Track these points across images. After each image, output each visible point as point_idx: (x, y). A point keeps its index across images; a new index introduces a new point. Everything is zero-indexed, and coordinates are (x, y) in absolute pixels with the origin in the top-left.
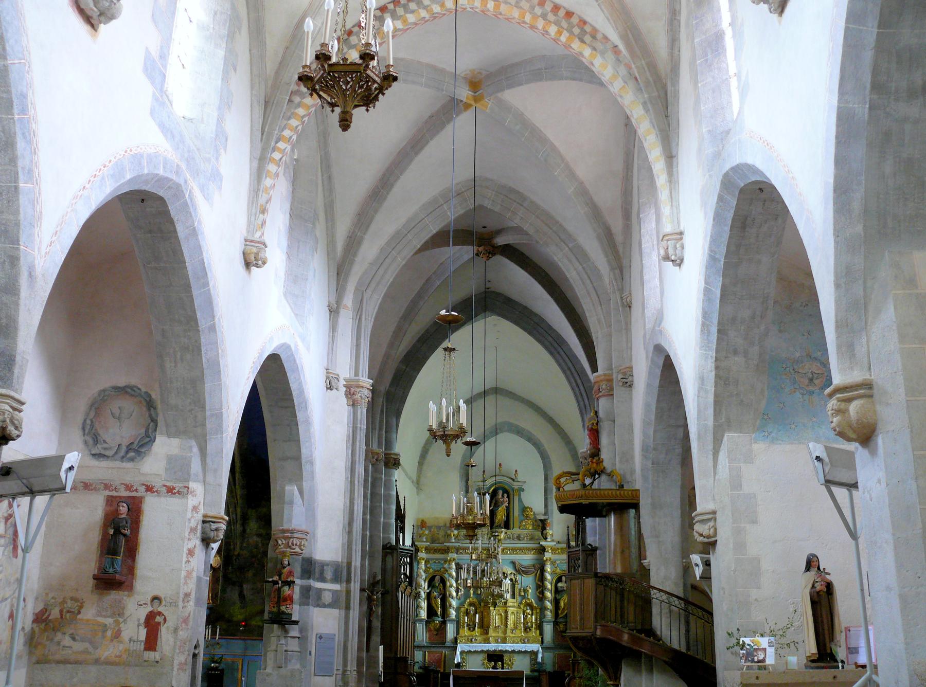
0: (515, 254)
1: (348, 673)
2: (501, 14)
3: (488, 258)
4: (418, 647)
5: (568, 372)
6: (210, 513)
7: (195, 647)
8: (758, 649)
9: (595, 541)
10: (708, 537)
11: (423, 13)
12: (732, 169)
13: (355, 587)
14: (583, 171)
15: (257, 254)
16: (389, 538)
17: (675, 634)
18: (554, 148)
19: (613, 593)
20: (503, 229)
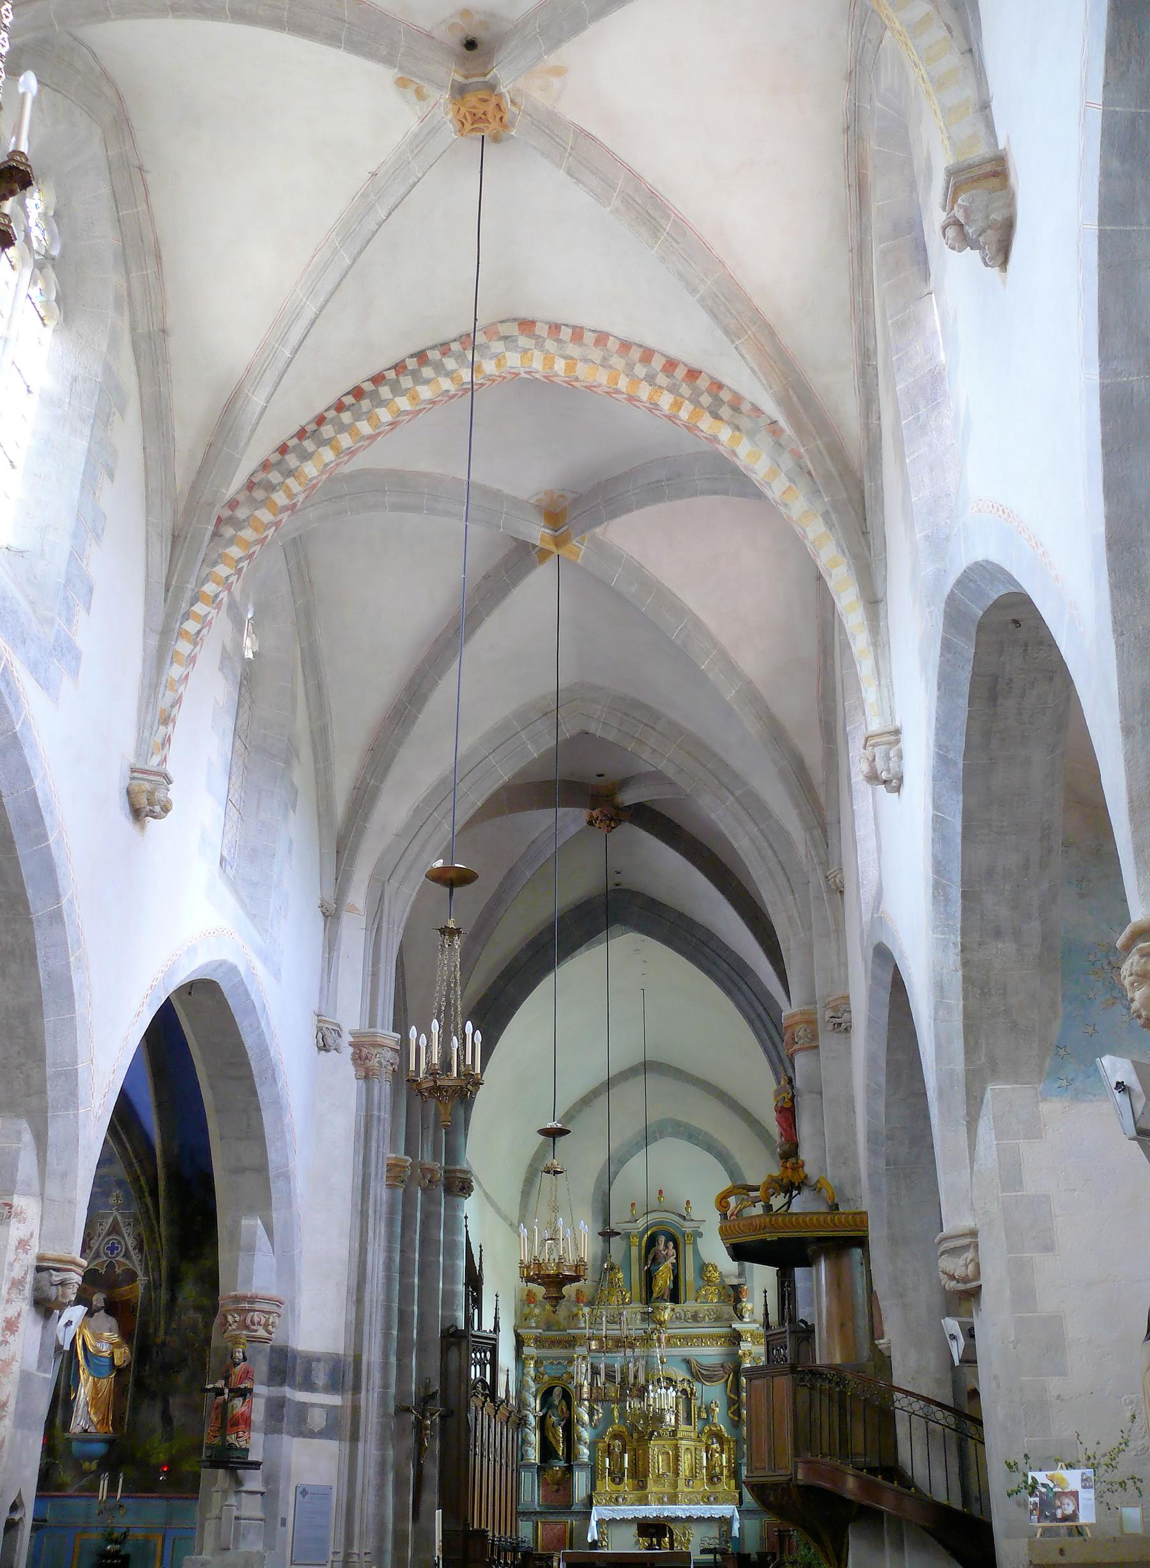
0: (651, 818)
1: (355, 1558)
2: (577, 379)
3: (610, 829)
4: (524, 1513)
5: (758, 1024)
6: (50, 1253)
7: (14, 1507)
8: (1063, 1494)
9: (811, 1315)
10: (965, 1280)
11: (446, 384)
12: (959, 582)
13: (370, 1402)
14: (752, 661)
15: (151, 793)
16: (456, 1319)
17: (938, 1474)
18: (698, 623)
19: (826, 1400)
20: (632, 777)
